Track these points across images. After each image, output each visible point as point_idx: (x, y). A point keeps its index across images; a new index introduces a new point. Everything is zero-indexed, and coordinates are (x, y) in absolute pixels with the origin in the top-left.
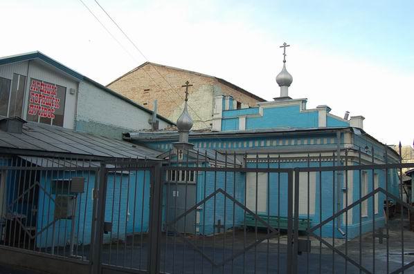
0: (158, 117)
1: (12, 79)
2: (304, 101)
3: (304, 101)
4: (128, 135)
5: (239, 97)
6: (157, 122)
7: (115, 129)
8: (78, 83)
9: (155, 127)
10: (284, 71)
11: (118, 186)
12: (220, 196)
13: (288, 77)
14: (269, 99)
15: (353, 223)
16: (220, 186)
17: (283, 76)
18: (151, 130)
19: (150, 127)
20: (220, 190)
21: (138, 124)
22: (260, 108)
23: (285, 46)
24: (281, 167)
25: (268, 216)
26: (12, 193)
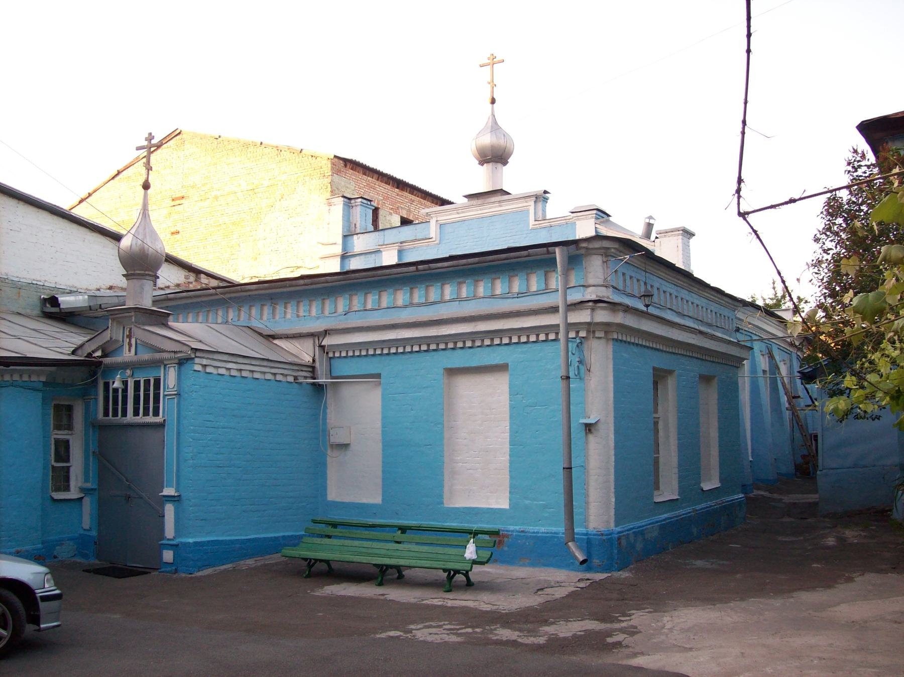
2: (542, 198)
3: (542, 198)
4: (54, 301)
5: (658, 282)
7: (18, 286)
10: (495, 127)
13: (502, 142)
14: (454, 193)
15: (616, 526)
17: (487, 140)
21: (89, 274)
22: (433, 222)
23: (493, 62)
26: (427, 559)
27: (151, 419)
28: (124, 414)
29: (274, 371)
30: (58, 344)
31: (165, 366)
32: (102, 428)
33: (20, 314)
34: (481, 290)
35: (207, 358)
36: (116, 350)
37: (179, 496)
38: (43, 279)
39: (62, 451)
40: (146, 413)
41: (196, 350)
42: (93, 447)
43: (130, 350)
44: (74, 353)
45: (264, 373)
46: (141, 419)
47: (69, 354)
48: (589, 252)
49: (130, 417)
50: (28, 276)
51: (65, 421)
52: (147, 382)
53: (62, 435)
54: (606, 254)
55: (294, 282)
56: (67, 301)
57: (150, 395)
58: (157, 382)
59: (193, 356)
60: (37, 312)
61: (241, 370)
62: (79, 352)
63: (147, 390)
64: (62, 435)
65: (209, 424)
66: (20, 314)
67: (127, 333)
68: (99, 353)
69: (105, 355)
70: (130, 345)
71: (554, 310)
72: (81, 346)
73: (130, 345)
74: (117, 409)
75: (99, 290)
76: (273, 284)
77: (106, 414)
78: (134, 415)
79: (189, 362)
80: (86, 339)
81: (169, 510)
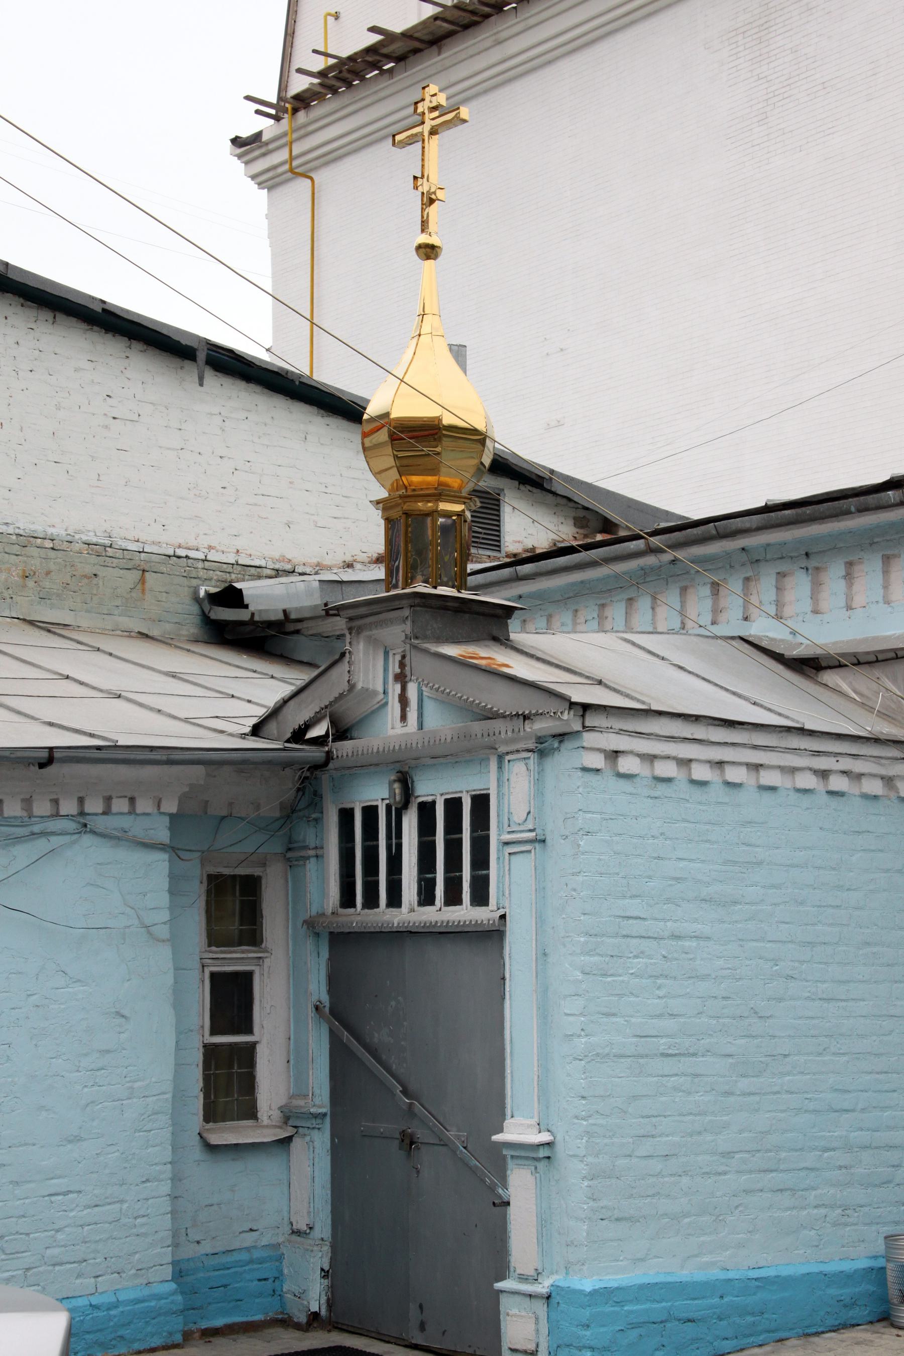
4: (231, 596)
27: (465, 913)
28: (395, 900)
29: (822, 763)
30: (222, 703)
31: (501, 758)
32: (342, 942)
33: (147, 636)
35: (621, 731)
36: (373, 712)
37: (549, 1144)
38: (203, 542)
39: (231, 1000)
40: (454, 898)
41: (586, 708)
42: (318, 988)
43: (404, 718)
44: (256, 730)
45: (793, 770)
46: (439, 914)
47: (243, 736)
49: (410, 912)
50: (164, 538)
51: (234, 926)
52: (453, 806)
53: (234, 960)
55: (871, 499)
56: (264, 597)
57: (462, 841)
58: (481, 803)
59: (577, 726)
60: (191, 626)
61: (720, 764)
62: (272, 727)
63: (395, 832)
64: (234, 960)
65: (635, 927)
66: (147, 636)
67: (394, 668)
68: (318, 731)
69: (341, 733)
70: (404, 701)
72: (275, 713)
73: (404, 701)
74: (377, 883)
75: (350, 566)
76: (808, 510)
77: (347, 899)
78: (421, 903)
79: (568, 745)
80: (286, 690)
81: (520, 1185)
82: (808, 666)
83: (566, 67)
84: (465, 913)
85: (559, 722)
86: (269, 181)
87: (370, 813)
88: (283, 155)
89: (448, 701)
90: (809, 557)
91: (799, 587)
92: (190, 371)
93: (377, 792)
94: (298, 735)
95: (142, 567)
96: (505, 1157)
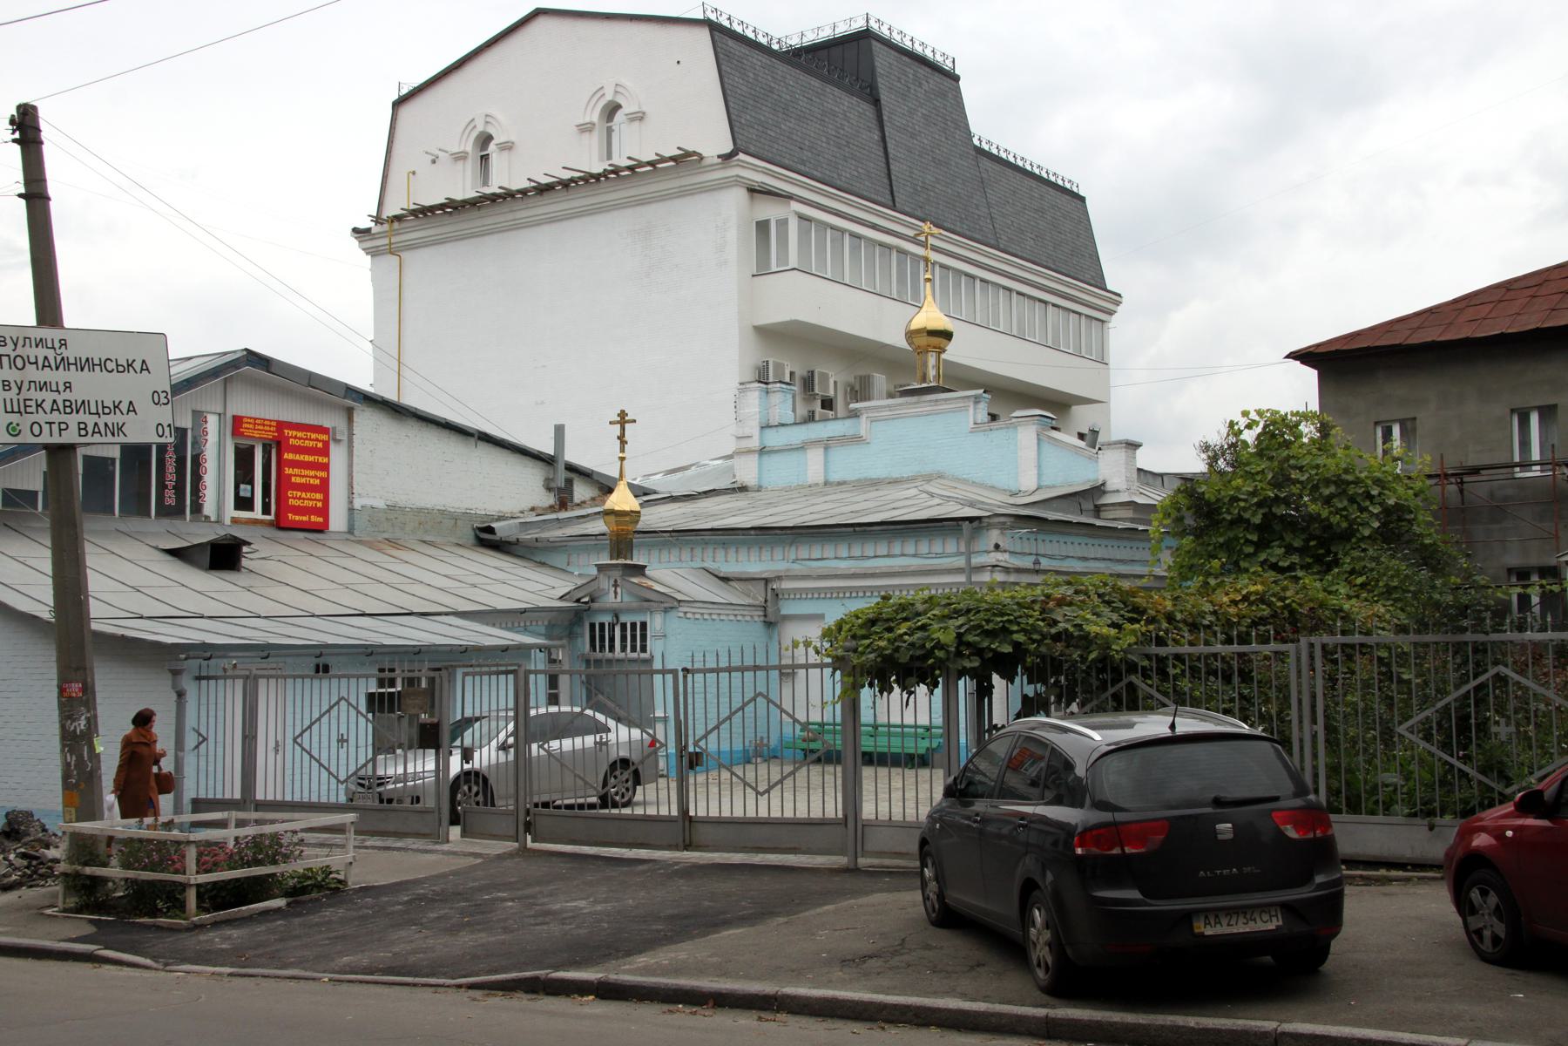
0: (571, 468)
1: (189, 425)
4: (490, 530)
6: (569, 482)
8: (350, 412)
9: (564, 501)
11: (883, 786)
12: (761, 789)
16: (761, 688)
18: (552, 509)
19: (550, 500)
20: (760, 694)
24: (698, 809)
25: (247, 801)
28: (612, 648)
34: (897, 549)
48: (990, 526)
54: (1003, 527)
58: (644, 625)
60: (471, 539)
69: (592, 600)
71: (959, 571)
82: (725, 579)
83: (546, 228)
84: (643, 655)
85: (669, 604)
86: (373, 253)
87: (602, 625)
88: (386, 241)
89: (630, 593)
90: (724, 545)
91: (720, 554)
92: (472, 440)
93: (607, 619)
94: (578, 601)
95: (455, 518)
96: (466, 776)
